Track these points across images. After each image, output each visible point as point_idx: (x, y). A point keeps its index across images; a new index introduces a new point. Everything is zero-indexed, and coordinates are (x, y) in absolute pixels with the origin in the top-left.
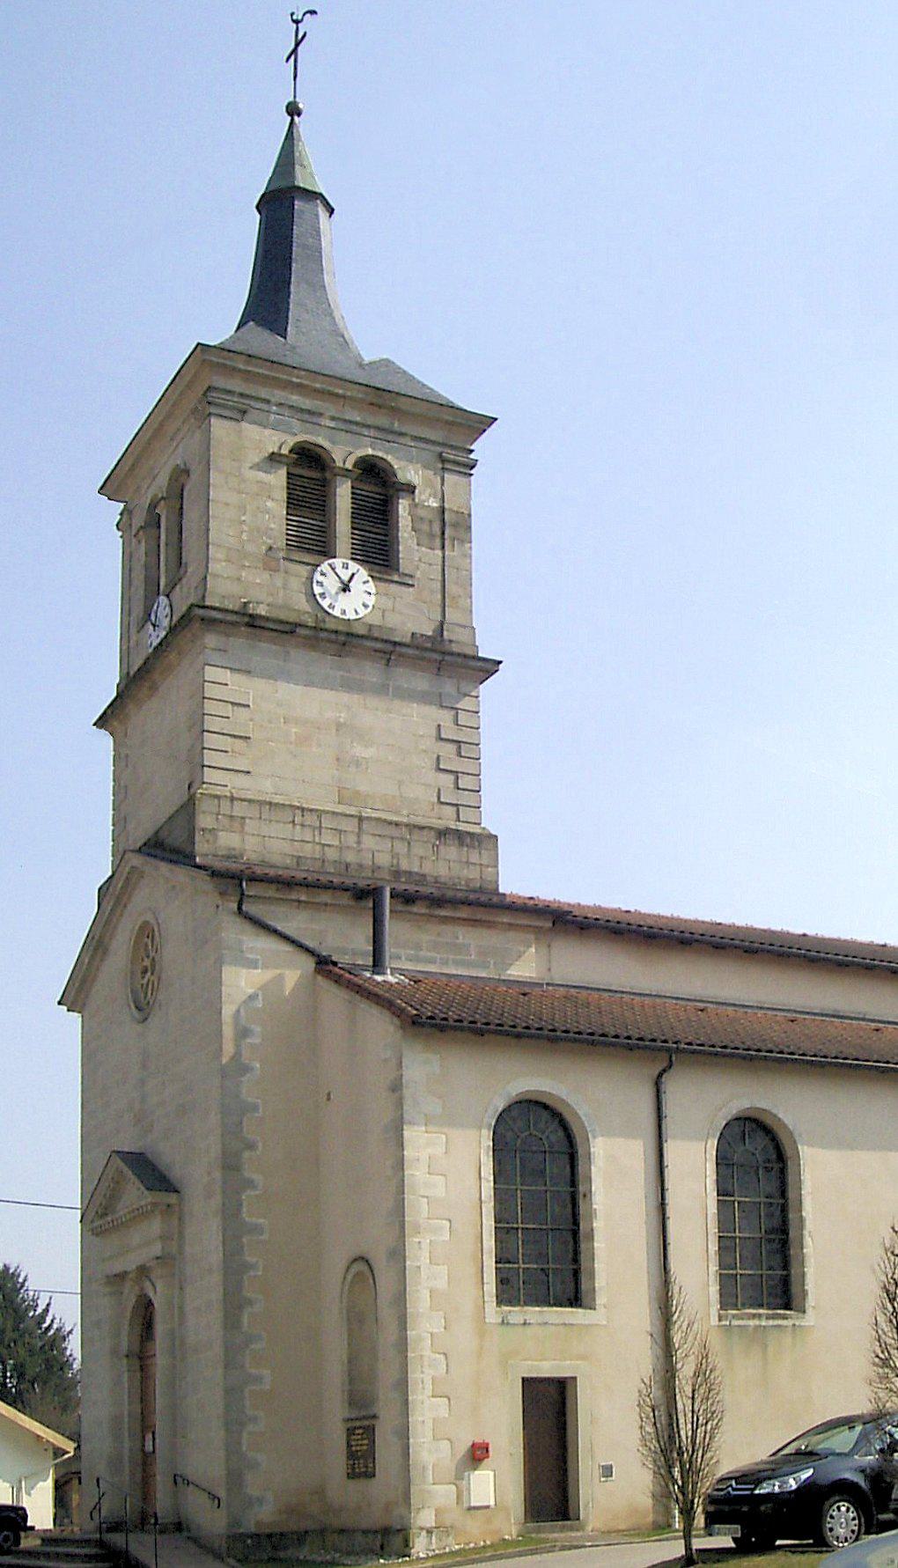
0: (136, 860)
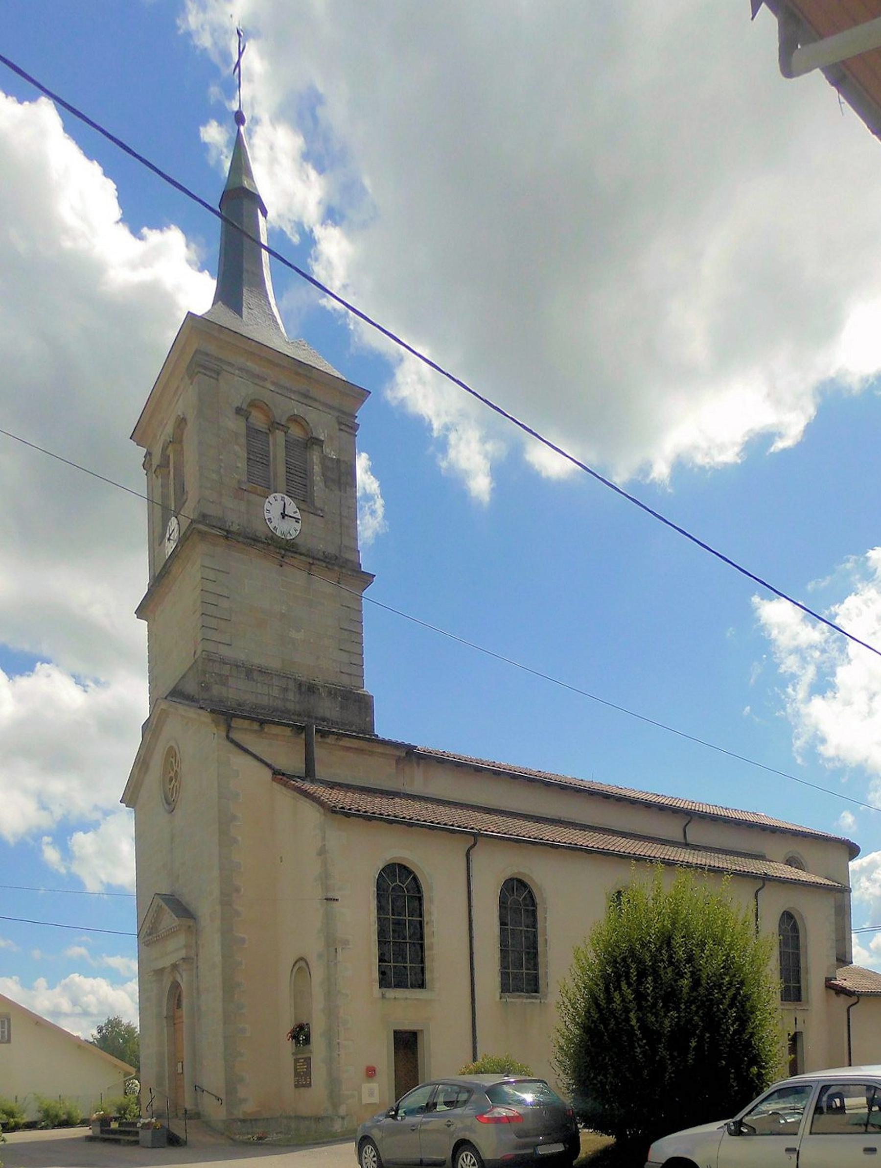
0: (163, 705)
